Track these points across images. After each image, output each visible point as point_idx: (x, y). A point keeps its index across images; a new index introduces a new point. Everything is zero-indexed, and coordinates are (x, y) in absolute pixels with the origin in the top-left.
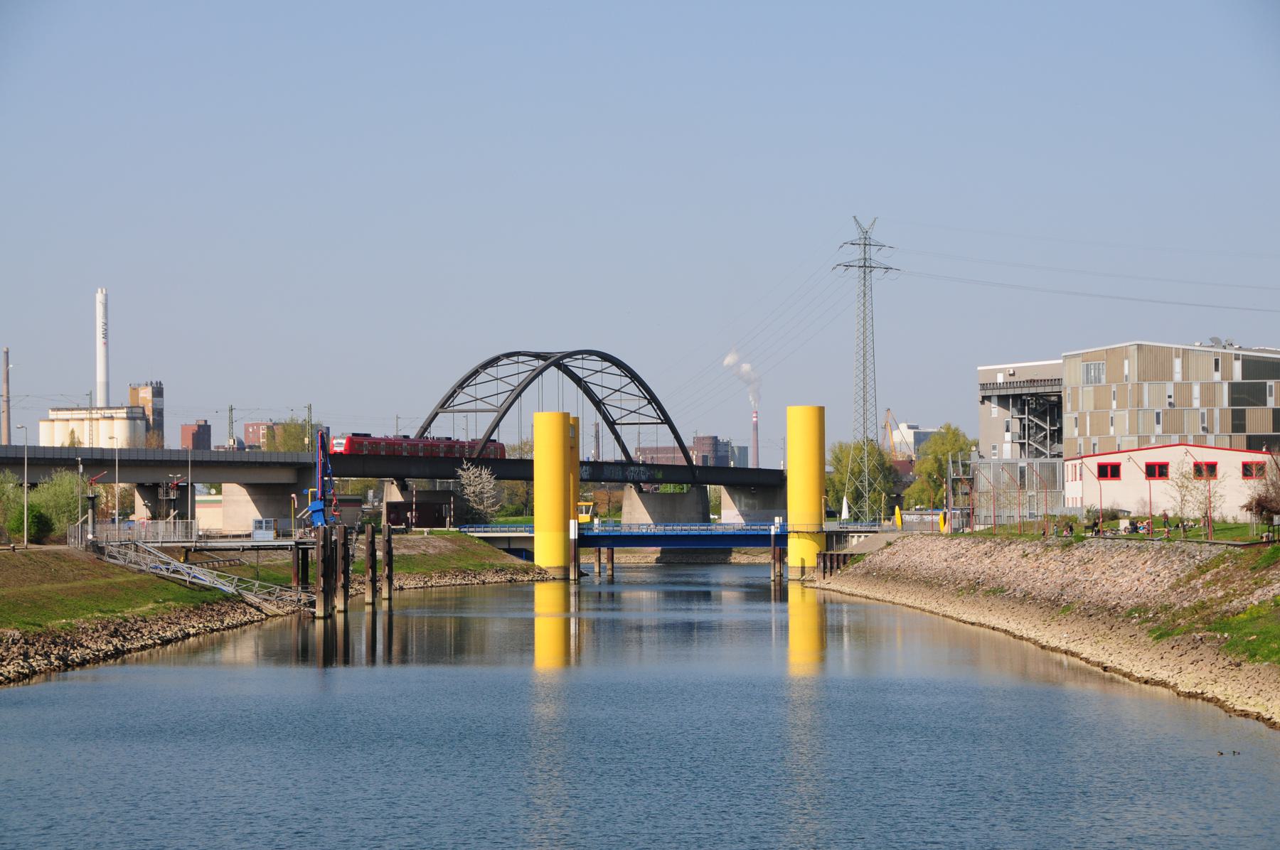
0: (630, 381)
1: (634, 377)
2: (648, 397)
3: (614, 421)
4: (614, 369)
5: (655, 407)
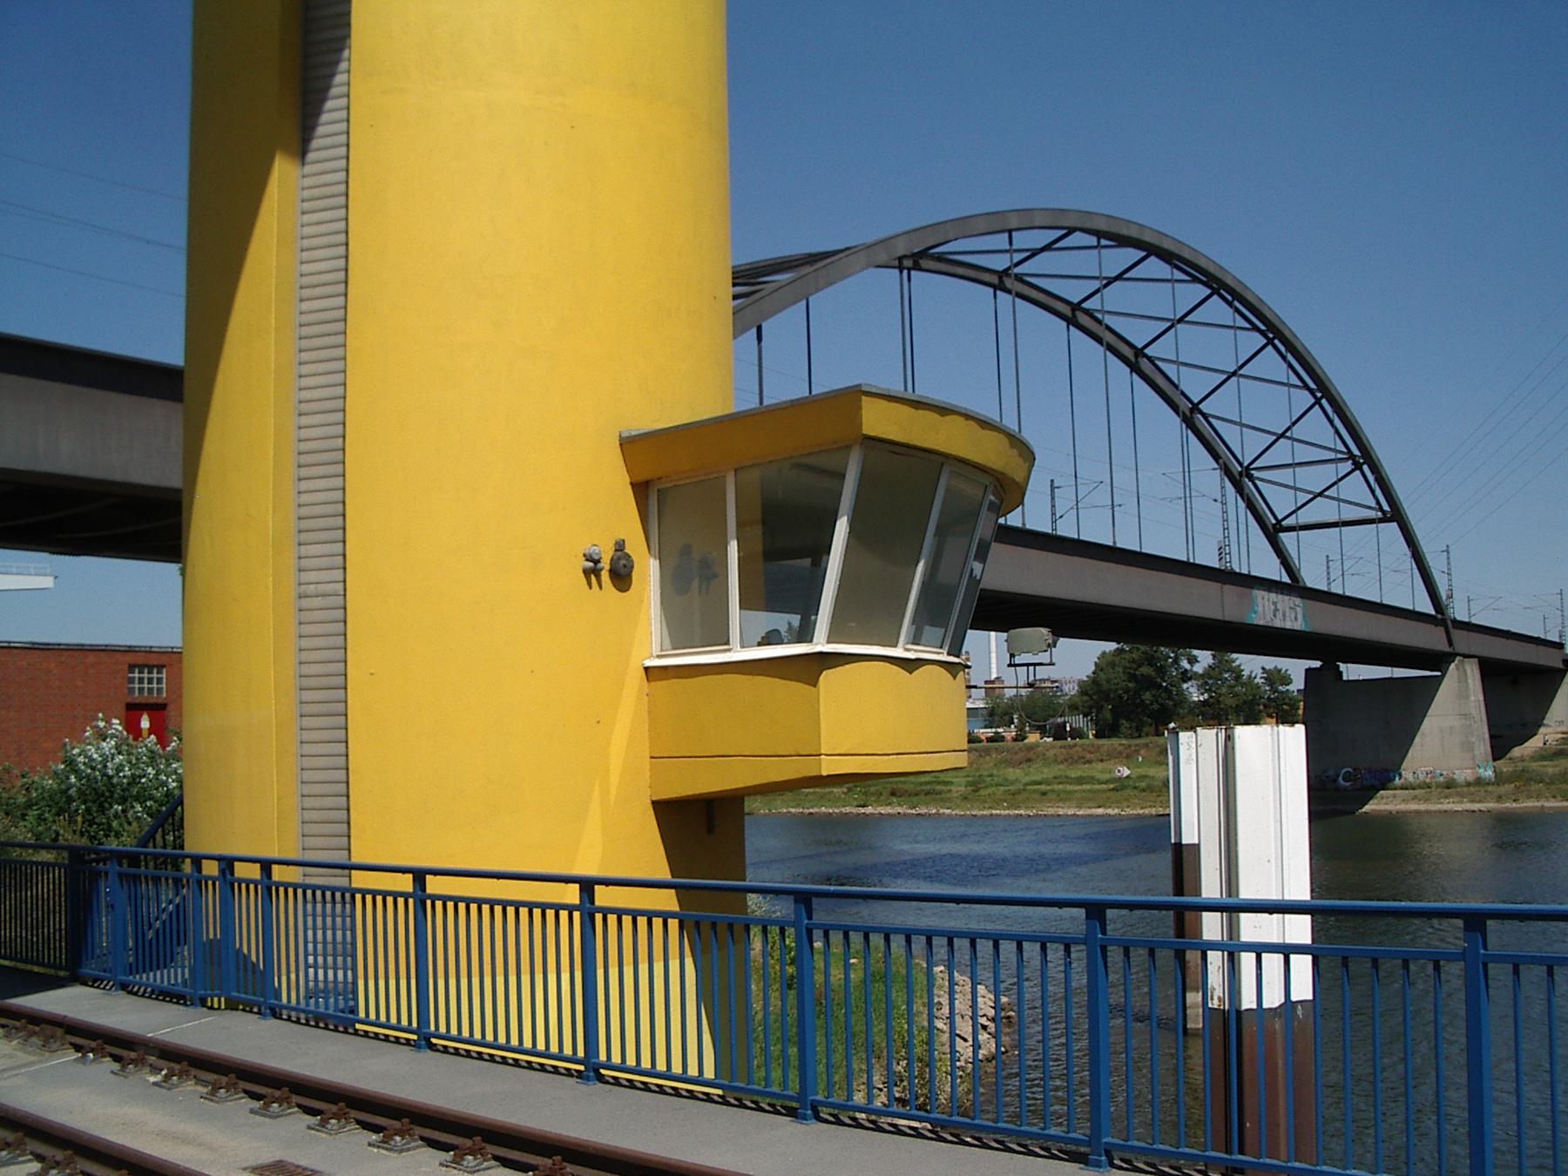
0: (1208, 291)
1: (1217, 285)
2: (1263, 328)
3: (1279, 522)
4: (1154, 266)
5: (1230, 298)
